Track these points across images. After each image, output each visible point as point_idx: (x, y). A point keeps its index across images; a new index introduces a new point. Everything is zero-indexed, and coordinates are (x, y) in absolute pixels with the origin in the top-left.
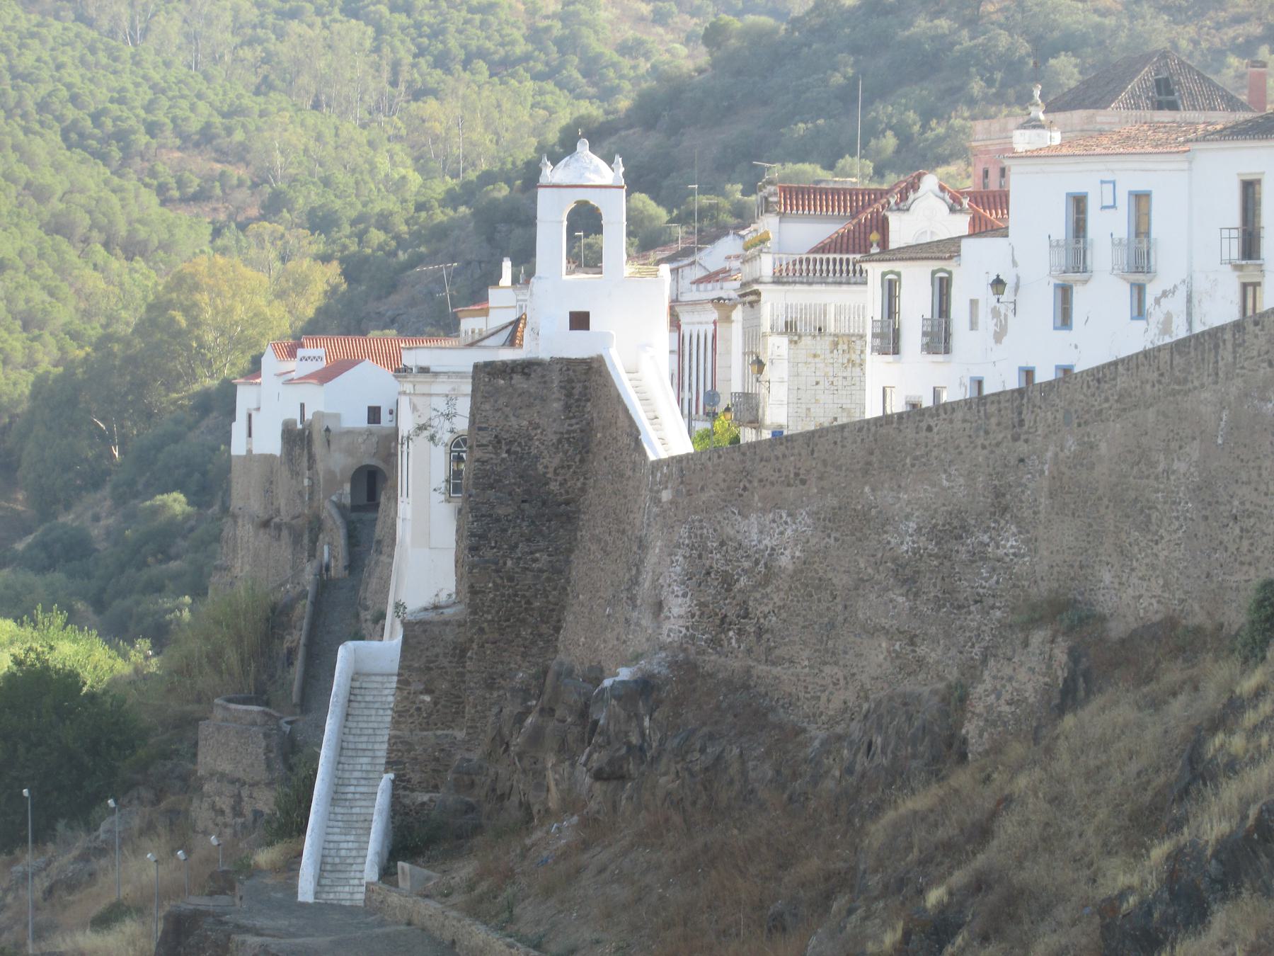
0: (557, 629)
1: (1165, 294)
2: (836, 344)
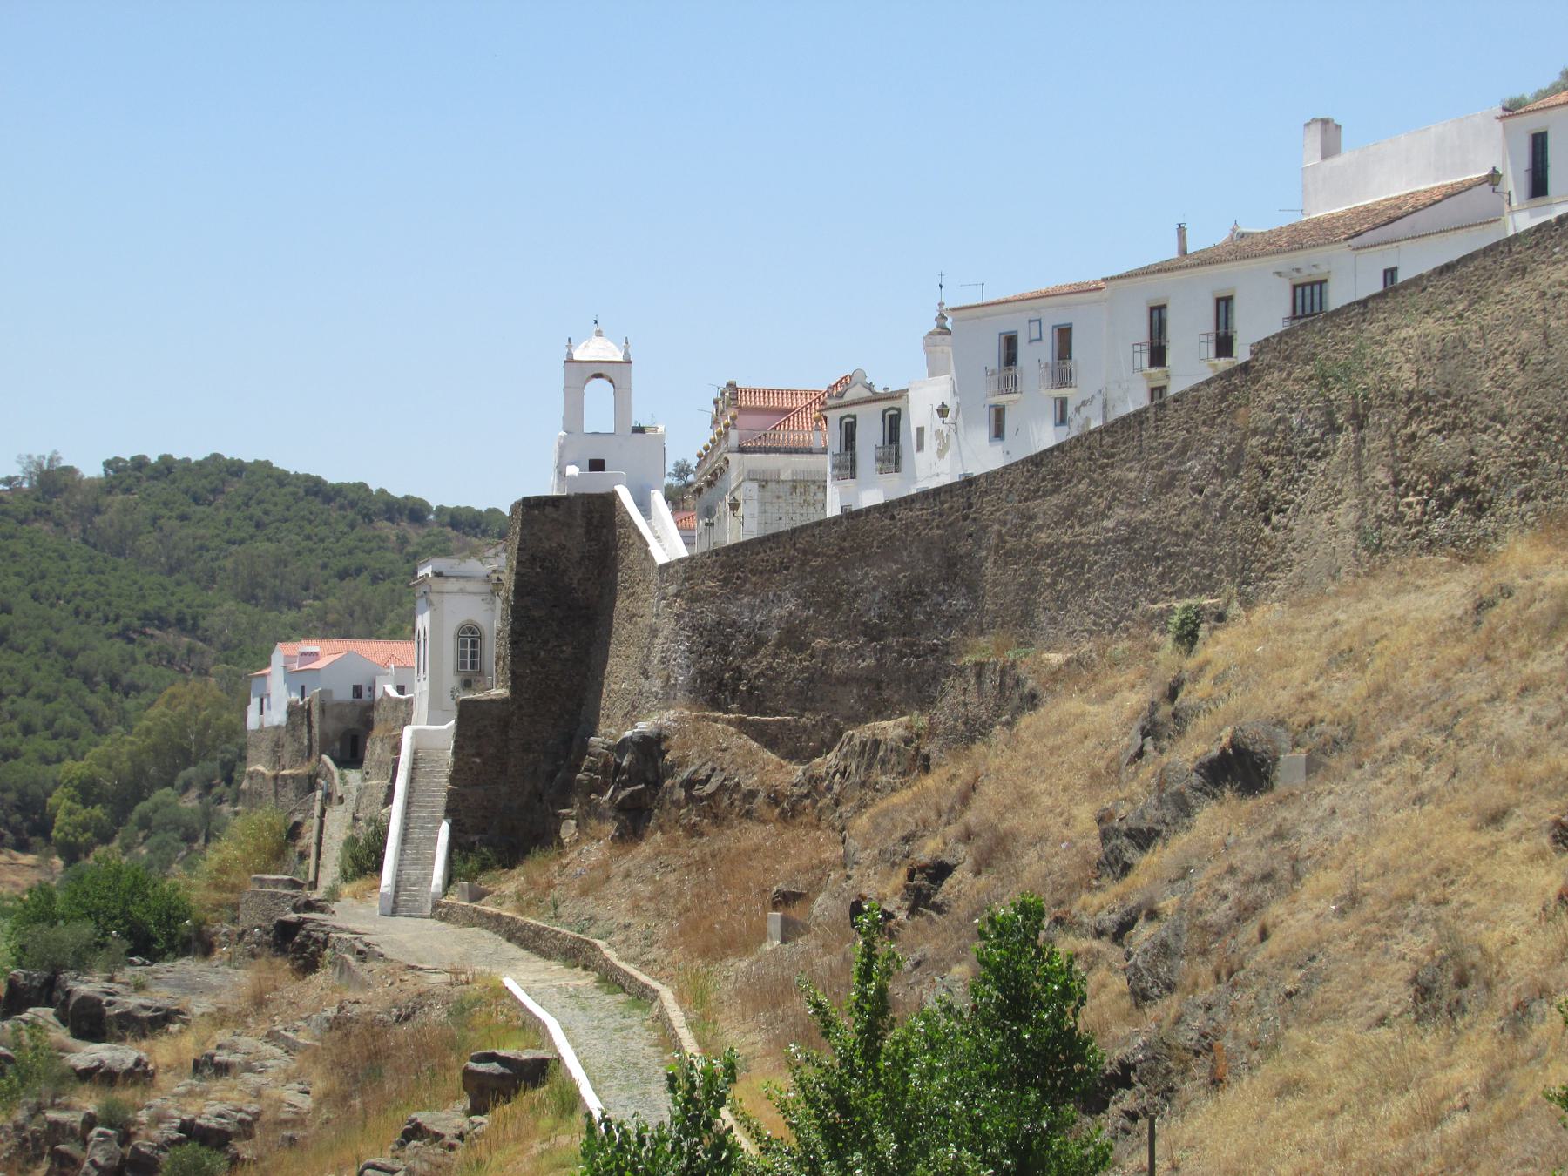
0: (580, 706)
1: (1084, 403)
2: (795, 488)
